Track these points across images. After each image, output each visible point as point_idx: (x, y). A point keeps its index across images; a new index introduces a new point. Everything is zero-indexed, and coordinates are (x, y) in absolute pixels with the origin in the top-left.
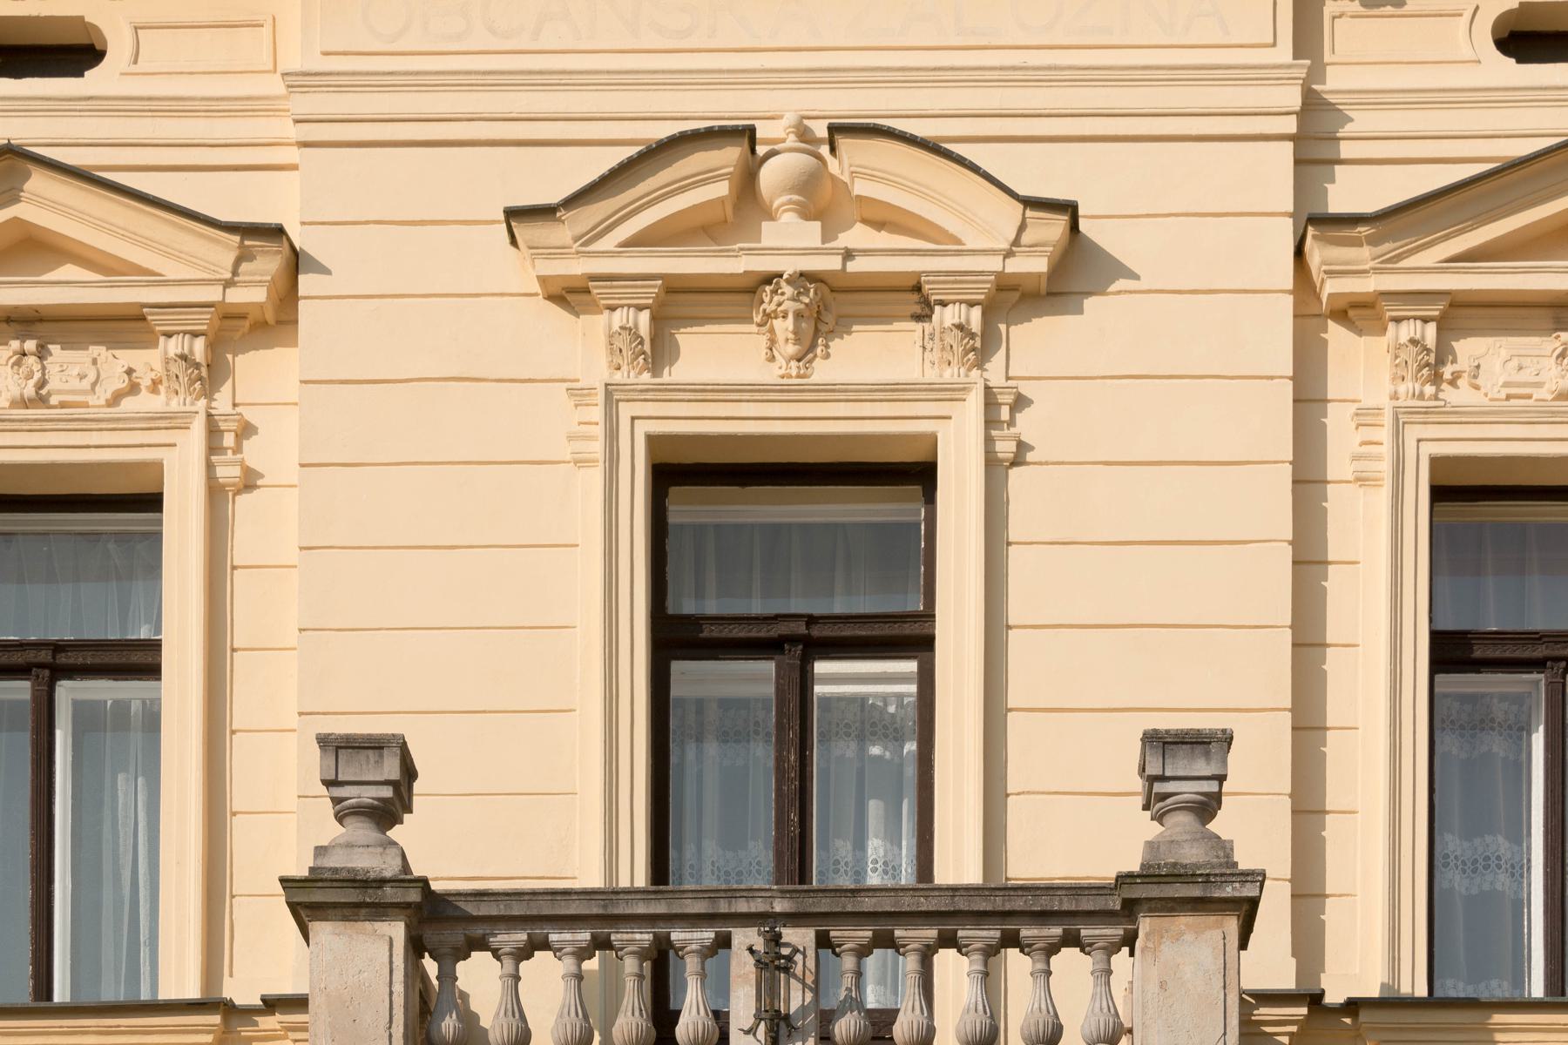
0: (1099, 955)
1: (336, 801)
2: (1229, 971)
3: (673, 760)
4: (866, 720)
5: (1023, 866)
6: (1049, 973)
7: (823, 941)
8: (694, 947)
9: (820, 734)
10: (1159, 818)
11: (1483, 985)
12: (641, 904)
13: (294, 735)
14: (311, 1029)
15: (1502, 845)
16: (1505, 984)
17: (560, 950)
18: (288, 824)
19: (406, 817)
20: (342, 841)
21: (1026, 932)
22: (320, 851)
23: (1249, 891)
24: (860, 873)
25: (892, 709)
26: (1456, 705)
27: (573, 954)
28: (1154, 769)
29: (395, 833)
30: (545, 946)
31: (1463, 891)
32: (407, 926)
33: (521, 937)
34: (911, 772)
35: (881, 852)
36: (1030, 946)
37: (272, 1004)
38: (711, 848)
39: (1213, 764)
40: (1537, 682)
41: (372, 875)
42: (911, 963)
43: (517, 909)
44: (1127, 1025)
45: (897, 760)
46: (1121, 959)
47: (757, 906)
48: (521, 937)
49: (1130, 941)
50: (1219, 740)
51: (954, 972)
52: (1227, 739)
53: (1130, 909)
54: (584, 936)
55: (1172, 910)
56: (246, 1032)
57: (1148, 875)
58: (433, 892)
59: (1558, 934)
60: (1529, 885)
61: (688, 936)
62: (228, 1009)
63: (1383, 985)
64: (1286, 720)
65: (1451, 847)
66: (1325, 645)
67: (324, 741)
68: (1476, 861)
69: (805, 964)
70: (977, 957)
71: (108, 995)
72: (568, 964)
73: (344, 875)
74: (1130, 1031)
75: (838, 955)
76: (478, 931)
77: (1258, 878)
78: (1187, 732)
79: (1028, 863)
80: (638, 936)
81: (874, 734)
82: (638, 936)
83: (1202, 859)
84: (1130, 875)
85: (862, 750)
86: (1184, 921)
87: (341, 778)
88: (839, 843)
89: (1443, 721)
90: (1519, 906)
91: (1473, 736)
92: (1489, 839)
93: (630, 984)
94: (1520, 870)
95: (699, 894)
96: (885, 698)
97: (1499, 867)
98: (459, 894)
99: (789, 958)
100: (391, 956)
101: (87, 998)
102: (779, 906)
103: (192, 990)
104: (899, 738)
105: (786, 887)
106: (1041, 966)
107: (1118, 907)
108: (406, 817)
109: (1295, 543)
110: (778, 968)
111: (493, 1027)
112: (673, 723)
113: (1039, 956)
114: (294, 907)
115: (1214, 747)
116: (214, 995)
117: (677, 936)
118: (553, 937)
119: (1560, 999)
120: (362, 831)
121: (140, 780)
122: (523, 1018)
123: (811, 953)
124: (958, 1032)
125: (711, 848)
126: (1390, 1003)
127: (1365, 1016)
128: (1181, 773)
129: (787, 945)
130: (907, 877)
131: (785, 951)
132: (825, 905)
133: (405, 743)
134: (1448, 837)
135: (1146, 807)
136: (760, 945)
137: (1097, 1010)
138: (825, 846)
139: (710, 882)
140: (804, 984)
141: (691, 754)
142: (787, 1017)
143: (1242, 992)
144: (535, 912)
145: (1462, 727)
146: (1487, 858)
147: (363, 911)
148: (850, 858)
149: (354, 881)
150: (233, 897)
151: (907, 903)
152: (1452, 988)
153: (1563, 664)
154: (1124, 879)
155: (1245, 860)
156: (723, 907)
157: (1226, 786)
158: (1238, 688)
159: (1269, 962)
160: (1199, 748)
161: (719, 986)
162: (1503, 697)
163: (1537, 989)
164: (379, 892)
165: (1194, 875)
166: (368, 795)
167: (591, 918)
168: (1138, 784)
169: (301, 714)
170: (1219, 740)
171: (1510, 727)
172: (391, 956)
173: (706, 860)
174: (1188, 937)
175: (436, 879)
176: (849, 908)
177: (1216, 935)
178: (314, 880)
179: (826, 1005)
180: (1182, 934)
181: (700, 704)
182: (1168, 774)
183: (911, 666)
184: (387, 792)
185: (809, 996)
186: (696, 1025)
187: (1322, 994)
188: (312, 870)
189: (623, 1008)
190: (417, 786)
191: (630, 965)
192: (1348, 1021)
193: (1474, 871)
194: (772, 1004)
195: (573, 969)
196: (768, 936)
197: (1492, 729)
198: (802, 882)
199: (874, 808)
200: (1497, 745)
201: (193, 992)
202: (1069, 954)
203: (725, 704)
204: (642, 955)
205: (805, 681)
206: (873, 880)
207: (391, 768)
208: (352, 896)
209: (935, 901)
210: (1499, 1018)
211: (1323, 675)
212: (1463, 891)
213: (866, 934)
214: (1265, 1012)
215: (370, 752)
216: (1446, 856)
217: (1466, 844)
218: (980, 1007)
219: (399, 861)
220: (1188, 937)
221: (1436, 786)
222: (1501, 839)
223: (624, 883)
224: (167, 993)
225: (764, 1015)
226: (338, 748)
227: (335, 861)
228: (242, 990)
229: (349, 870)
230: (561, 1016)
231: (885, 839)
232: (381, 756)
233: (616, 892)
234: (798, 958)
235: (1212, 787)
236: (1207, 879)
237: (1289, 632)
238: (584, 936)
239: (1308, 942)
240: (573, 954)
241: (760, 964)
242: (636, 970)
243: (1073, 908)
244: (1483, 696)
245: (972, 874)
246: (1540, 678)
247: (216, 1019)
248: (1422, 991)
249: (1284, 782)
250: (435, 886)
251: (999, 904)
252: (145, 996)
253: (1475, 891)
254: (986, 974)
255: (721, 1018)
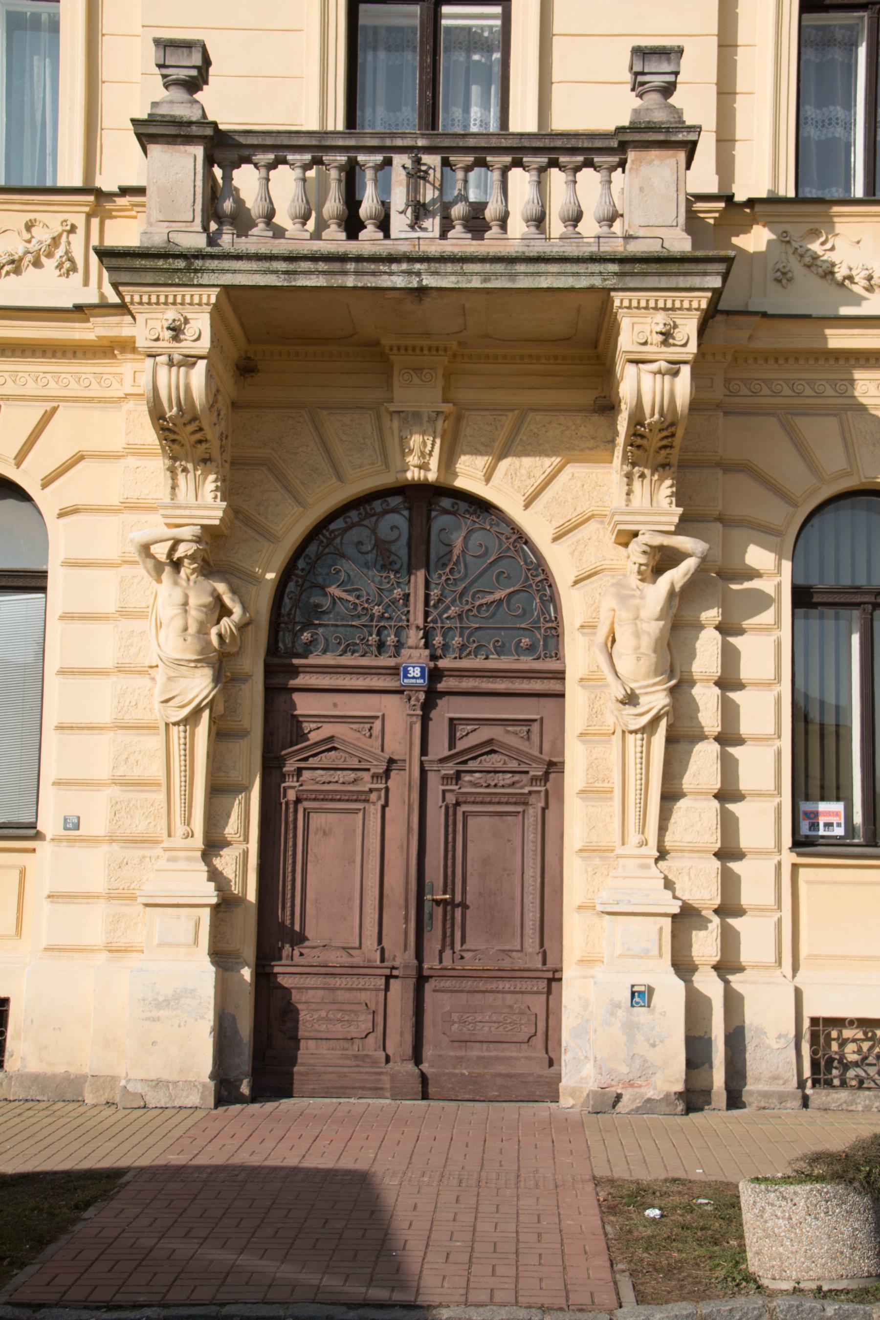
0: (605, 172)
1: (164, 76)
2: (679, 182)
3: (360, 60)
4: (471, 40)
5: (560, 123)
6: (575, 182)
7: (445, 163)
8: (371, 165)
9: (445, 48)
10: (640, 96)
11: (826, 191)
12: (341, 140)
13: (139, 39)
14: (147, 205)
15: (839, 111)
16: (840, 190)
17: (293, 164)
18: (136, 88)
19: (205, 87)
20: (167, 99)
21: (563, 159)
22: (155, 104)
23: (692, 137)
24: (466, 126)
25: (486, 34)
26: (814, 32)
27: (301, 167)
28: (638, 68)
29: (198, 96)
30: (285, 162)
31: (816, 138)
32: (205, 149)
33: (271, 156)
34: (497, 70)
35: (479, 115)
36: (564, 167)
37: (124, 191)
38: (381, 111)
39: (672, 65)
40: (863, 17)
41: (185, 119)
42: (496, 176)
43: (269, 141)
44: (620, 212)
45: (488, 63)
46: (617, 174)
47: (408, 142)
48: (271, 156)
49: (622, 164)
50: (676, 52)
51: (521, 181)
52: (680, 51)
53: (623, 147)
54: (307, 157)
55: (647, 147)
56: (109, 206)
57: (634, 128)
58: (220, 130)
59: (872, 161)
60: (855, 134)
61: (367, 158)
62: (98, 193)
63: (769, 191)
64: (715, 40)
65: (809, 113)
66: (735, 141)
67: (158, 42)
68: (823, 121)
69: (435, 175)
70: (534, 173)
71: (27, 183)
72: (298, 172)
73: (168, 119)
74: (622, 216)
75: (454, 171)
76: (246, 152)
77: (697, 129)
78: (657, 47)
79: (564, 120)
80: (338, 158)
81: (476, 48)
82: (338, 158)
83: (665, 119)
84: (623, 128)
85: (469, 57)
86: (654, 154)
87: (167, 63)
88: (455, 109)
89: (806, 41)
90: (848, 146)
91: (823, 50)
92: (832, 108)
93: (334, 185)
94: (849, 126)
95: (374, 135)
96: (482, 28)
97: (837, 124)
98: (235, 132)
99: (426, 172)
100: (195, 165)
101: (14, 184)
102: (421, 143)
103: (77, 182)
104: (490, 50)
105: (424, 132)
106: (571, 178)
107: (616, 145)
108: (205, 87)
109: (718, 84)
110: (420, 177)
111: (254, 207)
112: (360, 39)
113: (570, 173)
114: (139, 136)
115: (673, 56)
116: (90, 186)
117: (361, 158)
118: (290, 157)
119: (873, 198)
120: (178, 94)
121: (47, 60)
122: (271, 202)
123: (438, 169)
124: (522, 214)
125: (381, 111)
126: (773, 200)
127: (758, 208)
128: (653, 70)
129: (425, 164)
130: (493, 127)
131: (424, 168)
132: (447, 143)
133: (204, 45)
134: (808, 107)
135: (633, 90)
136: (409, 164)
137: (603, 203)
138: (446, 110)
139: (379, 129)
140: (434, 187)
141: (370, 57)
142: (424, 205)
143: (687, 194)
144: (279, 143)
145: (817, 44)
146: (830, 119)
147: (179, 139)
148: (460, 118)
149: (174, 122)
150: (102, 129)
151: (494, 142)
152: (810, 192)
153: (878, 6)
154: (620, 130)
155: (689, 120)
156: (388, 142)
157: (680, 79)
158: (689, 23)
159: (703, 177)
160: (664, 57)
161: (384, 188)
162: (842, 27)
163: (858, 191)
164: (189, 129)
165: (660, 128)
166: (183, 74)
167: (314, 147)
168: (628, 77)
169: (143, 26)
170: (676, 52)
171: (845, 44)
172: (195, 165)
173: (376, 117)
174: (657, 163)
175: (222, 123)
176: (461, 144)
177: (673, 161)
178: (151, 120)
179: (448, 198)
180: (652, 161)
181: (375, 29)
182: (646, 71)
183: (497, 10)
184: (194, 73)
185: (437, 193)
186: (371, 208)
187: (733, 196)
188: (149, 115)
189: (329, 198)
190: (212, 70)
191: (334, 174)
192: (748, 210)
193: (823, 126)
194: (415, 197)
195: (301, 175)
196: (414, 159)
197: (835, 45)
198: (433, 129)
199: (475, 90)
200: (837, 54)
201: (78, 183)
202: (587, 172)
203: (390, 29)
204: (340, 168)
205: (436, 17)
206: (474, 129)
207: (196, 59)
208: (172, 131)
209: (510, 141)
210: (836, 209)
211: (734, 110)
212: (816, 138)
213: (470, 159)
214: (699, 206)
215: (185, 50)
216: (806, 118)
217: (818, 112)
218: (536, 201)
219: (200, 112)
220: (657, 163)
221: (802, 78)
222: (839, 108)
223: (331, 128)
224: (62, 183)
225: (411, 203)
226: (165, 46)
227: (163, 110)
228: (107, 182)
229: (171, 116)
230: (293, 201)
231: (481, 107)
232: (191, 52)
233: (326, 133)
234: (431, 172)
235: (671, 78)
236: (668, 130)
237: (714, 134)
238: (307, 157)
239: (725, 166)
240: (301, 167)
241: (409, 175)
242: (337, 177)
243: (590, 146)
244: (830, 26)
245: (532, 127)
246: (865, 15)
247: (91, 198)
248: (791, 194)
249: (712, 76)
250: (221, 127)
251: (547, 143)
252: (49, 183)
253: (823, 138)
254: (539, 183)
255: (385, 206)
